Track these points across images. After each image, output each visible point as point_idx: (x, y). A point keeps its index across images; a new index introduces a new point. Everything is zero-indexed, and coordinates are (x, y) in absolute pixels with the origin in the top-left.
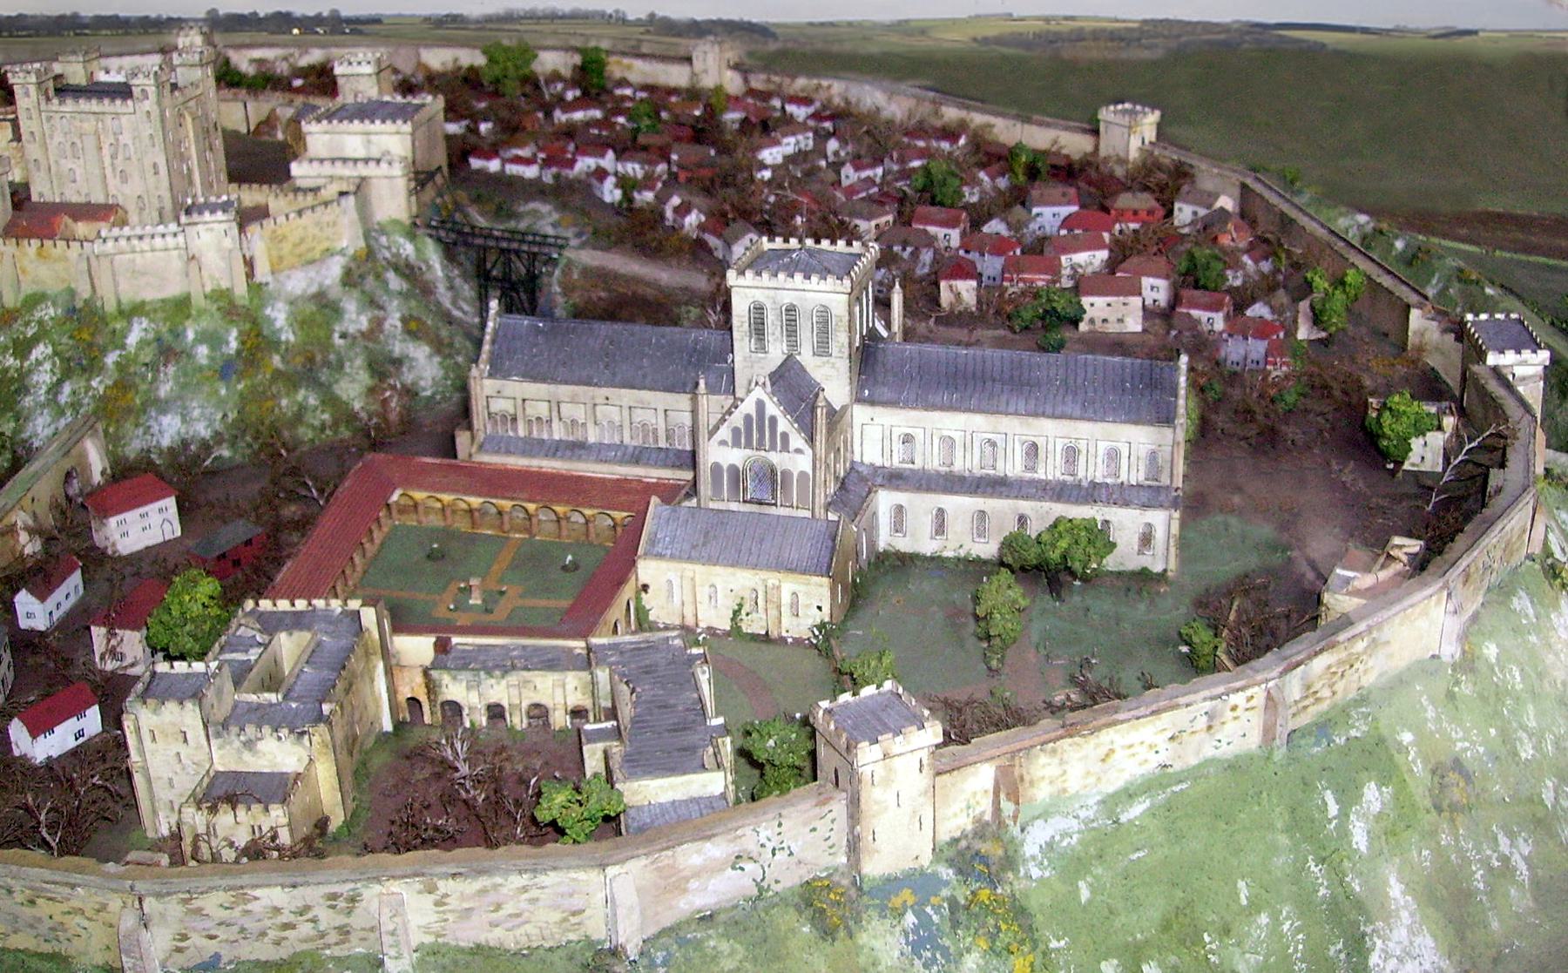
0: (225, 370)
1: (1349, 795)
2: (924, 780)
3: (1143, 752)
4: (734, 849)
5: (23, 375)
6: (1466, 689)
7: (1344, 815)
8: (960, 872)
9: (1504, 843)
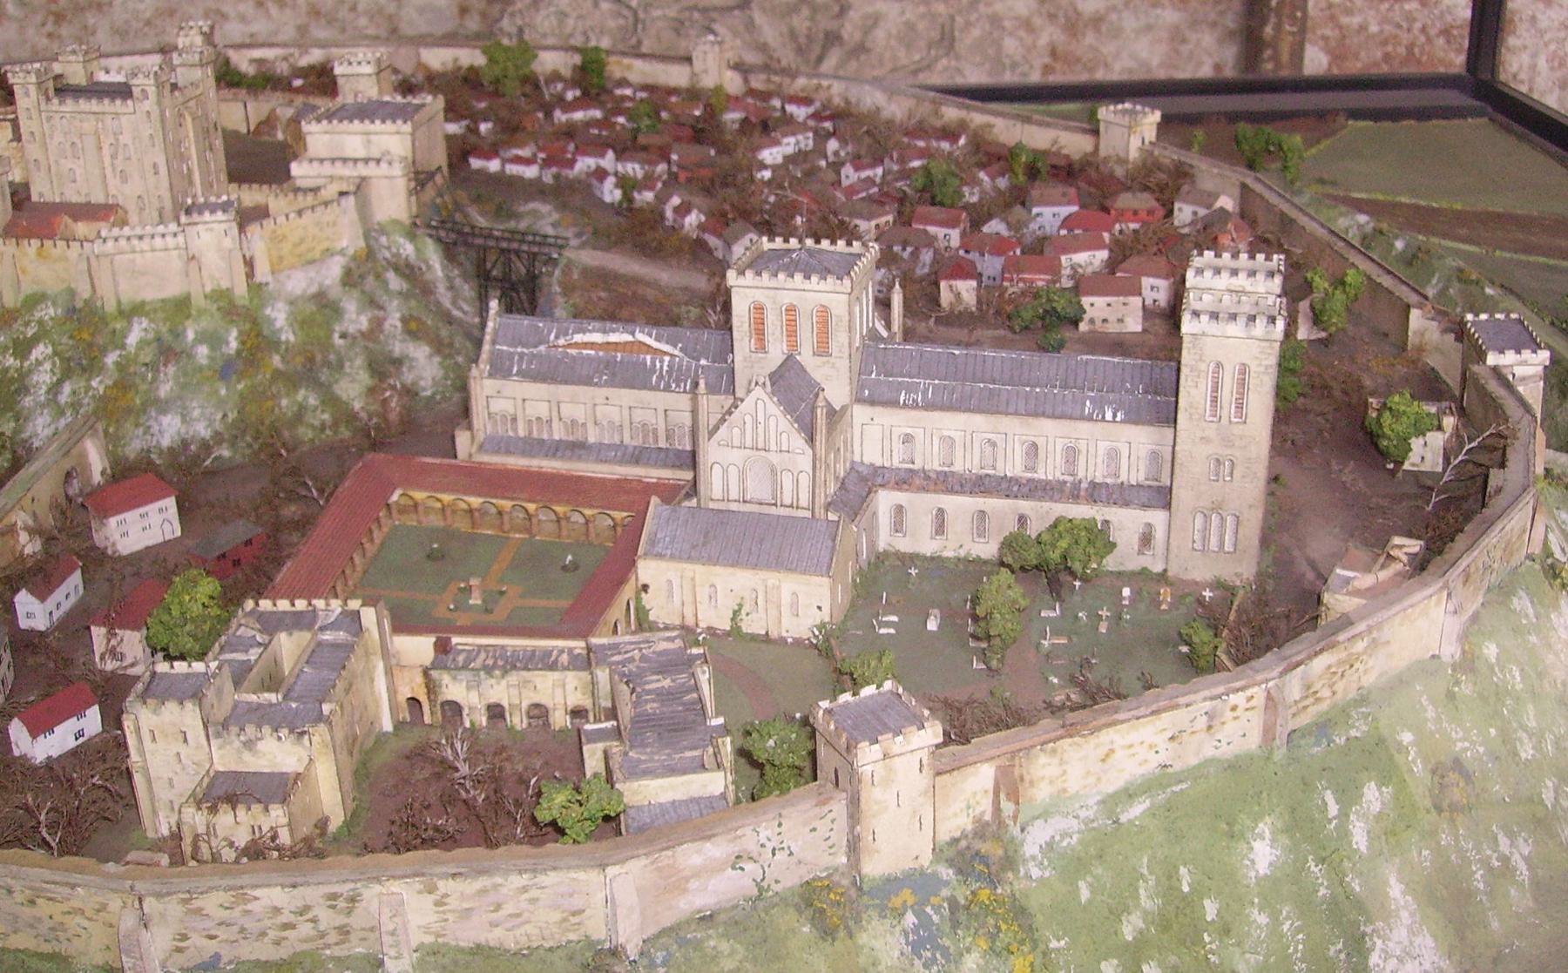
0: (226, 370)
1: (1349, 795)
2: (924, 780)
4: (735, 848)
5: (23, 375)
6: (1466, 689)
7: (1344, 815)
8: (960, 872)
9: (1504, 843)
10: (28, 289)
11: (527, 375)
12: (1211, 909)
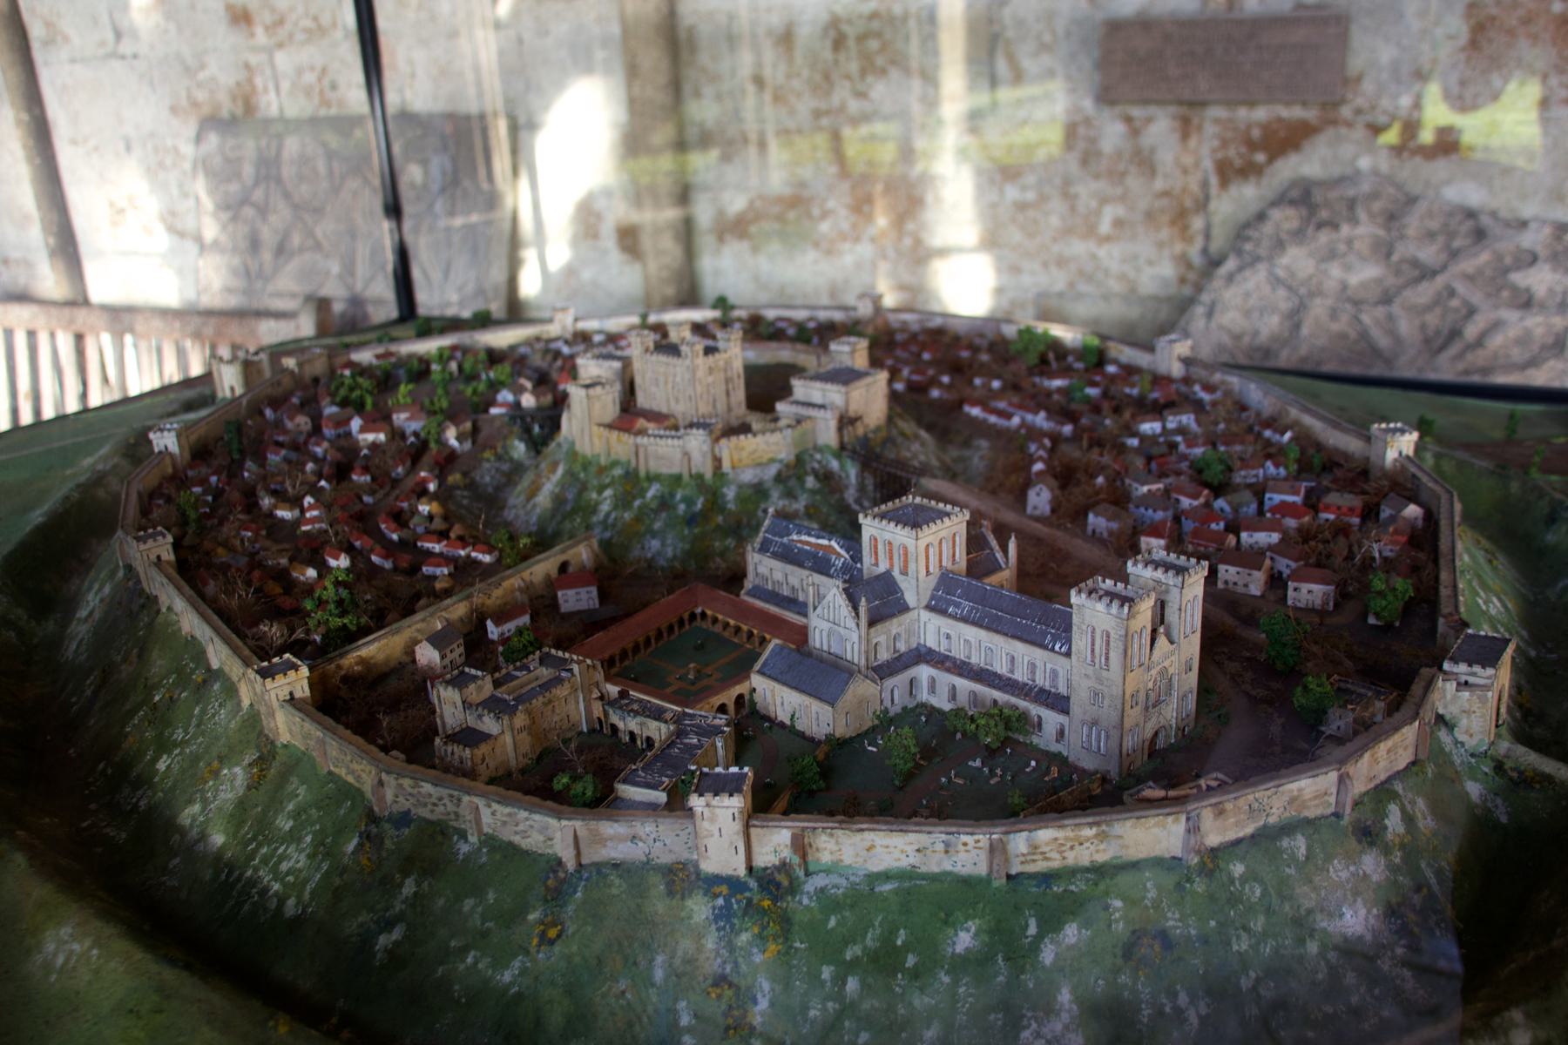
0: (691, 520)
2: (737, 826)
3: (897, 854)
4: (631, 832)
5: (597, 504)
6: (1199, 886)
7: (1039, 937)
8: (760, 886)
10: (613, 457)
11: (775, 556)
12: (911, 960)
